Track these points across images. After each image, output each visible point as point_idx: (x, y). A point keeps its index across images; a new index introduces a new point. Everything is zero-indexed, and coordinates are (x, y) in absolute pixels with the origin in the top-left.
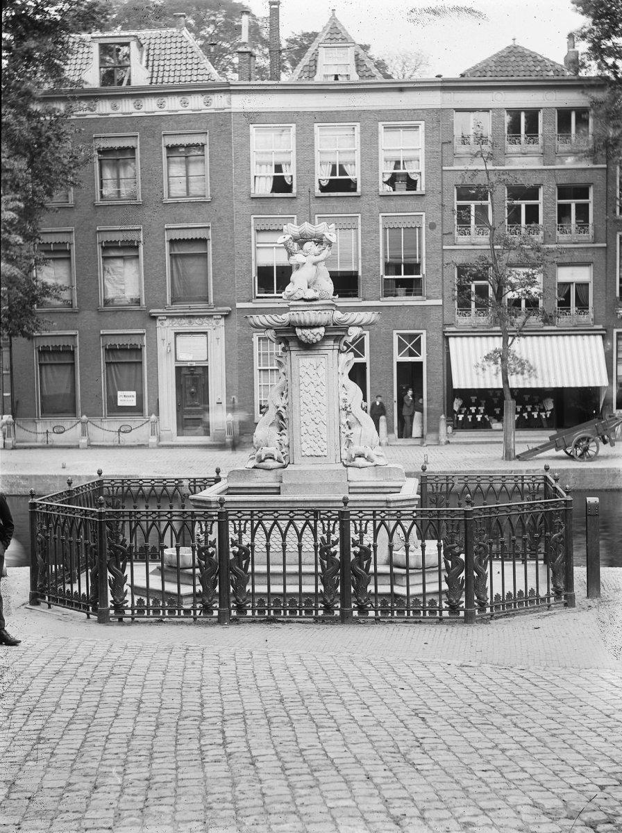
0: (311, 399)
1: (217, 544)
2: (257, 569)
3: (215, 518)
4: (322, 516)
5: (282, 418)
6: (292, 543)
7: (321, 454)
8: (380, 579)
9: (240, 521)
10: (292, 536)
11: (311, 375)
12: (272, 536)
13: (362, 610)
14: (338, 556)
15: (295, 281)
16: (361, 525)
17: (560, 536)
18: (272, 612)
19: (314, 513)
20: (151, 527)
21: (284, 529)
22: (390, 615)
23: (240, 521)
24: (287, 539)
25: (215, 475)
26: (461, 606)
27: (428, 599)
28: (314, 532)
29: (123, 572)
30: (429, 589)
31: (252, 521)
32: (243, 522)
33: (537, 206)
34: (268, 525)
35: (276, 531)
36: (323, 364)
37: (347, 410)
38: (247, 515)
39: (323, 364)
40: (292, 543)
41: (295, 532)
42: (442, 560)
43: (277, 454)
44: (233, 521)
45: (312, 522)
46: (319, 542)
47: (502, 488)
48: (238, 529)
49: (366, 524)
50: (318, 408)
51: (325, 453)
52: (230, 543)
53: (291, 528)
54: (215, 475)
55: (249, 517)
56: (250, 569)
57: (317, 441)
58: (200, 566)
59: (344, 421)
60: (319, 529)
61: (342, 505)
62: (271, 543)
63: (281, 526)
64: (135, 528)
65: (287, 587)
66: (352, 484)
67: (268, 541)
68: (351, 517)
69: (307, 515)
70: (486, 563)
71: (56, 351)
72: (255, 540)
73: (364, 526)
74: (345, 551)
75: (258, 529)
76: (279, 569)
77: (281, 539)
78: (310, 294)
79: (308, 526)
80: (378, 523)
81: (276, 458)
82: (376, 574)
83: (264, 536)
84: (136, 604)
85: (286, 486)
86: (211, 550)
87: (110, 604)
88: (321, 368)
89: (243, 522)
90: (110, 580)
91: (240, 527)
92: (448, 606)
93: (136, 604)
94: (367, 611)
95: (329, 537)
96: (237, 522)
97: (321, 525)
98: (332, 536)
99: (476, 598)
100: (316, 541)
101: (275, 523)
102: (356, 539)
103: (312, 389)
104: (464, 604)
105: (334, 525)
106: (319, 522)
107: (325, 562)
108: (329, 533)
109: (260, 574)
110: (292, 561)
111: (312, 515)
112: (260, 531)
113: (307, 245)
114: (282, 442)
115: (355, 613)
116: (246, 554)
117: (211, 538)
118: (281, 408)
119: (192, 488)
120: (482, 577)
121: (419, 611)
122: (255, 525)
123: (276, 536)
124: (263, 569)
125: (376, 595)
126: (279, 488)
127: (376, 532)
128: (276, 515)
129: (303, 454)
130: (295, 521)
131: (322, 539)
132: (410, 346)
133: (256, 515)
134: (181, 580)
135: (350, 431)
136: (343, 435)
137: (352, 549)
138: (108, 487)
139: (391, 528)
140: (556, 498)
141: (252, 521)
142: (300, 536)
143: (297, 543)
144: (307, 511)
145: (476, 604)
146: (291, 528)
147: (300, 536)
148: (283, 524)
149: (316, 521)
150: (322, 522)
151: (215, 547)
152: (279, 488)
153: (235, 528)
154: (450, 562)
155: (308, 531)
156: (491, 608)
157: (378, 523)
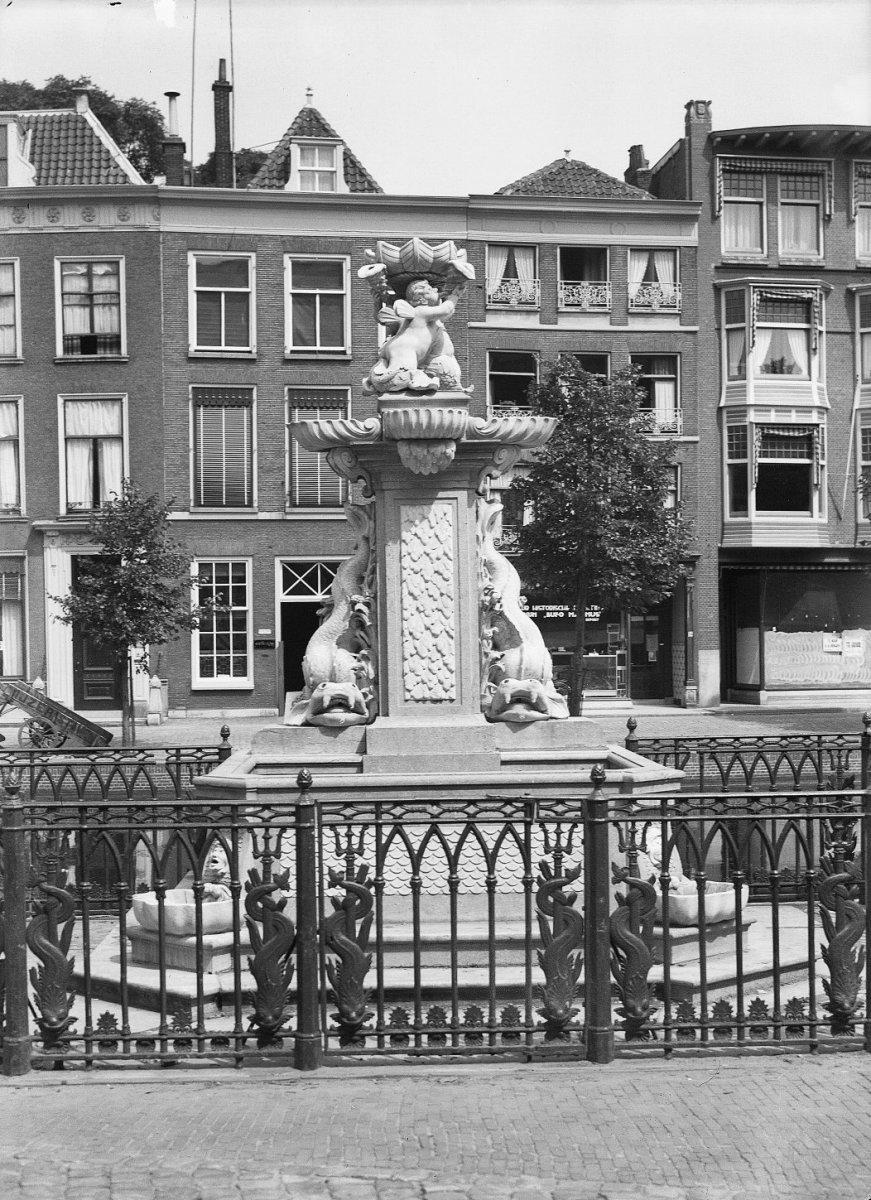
0: (423, 585)
2: (389, 934)
4: (543, 813)
5: (361, 625)
6: (433, 875)
7: (444, 695)
8: (389, 958)
9: (267, 829)
10: (472, 853)
12: (462, 859)
13: (350, 1033)
14: (578, 906)
18: (424, 1038)
21: (491, 845)
22: (195, 1050)
23: (267, 829)
24: (498, 866)
25: (219, 741)
26: (286, 1026)
27: (713, 996)
28: (525, 848)
29: (65, 951)
31: (379, 827)
32: (565, 827)
34: (416, 834)
36: (450, 517)
37: (490, 612)
40: (433, 875)
42: (534, 915)
43: (354, 694)
45: (520, 829)
46: (536, 872)
48: (344, 846)
49: (362, 834)
51: (453, 694)
52: (611, 875)
53: (434, 843)
54: (219, 741)
56: (373, 935)
57: (435, 669)
59: (488, 632)
60: (537, 846)
62: (460, 874)
63: (412, 839)
65: (386, 972)
67: (491, 869)
69: (508, 809)
72: (385, 869)
76: (443, 932)
77: (484, 867)
78: (421, 380)
79: (509, 836)
80: (387, 830)
81: (352, 702)
82: (382, 946)
84: (95, 1027)
85: (375, 760)
87: (615, 1017)
89: (356, 830)
91: (349, 842)
92: (544, 1020)
93: (95, 1027)
94: (363, 1037)
95: (558, 860)
96: (551, 827)
97: (541, 836)
98: (566, 857)
100: (528, 869)
101: (434, 830)
102: (337, 870)
105: (571, 832)
106: (535, 828)
108: (558, 853)
109: (397, 946)
110: (471, 916)
111: (518, 810)
112: (397, 849)
115: (334, 1044)
116: (363, 898)
119: (173, 768)
121: (517, 1034)
122: (384, 840)
123: (435, 859)
124: (406, 934)
127: (381, 852)
131: (253, 873)
132: (300, 579)
134: (168, 960)
135: (497, 654)
137: (613, 889)
138: (188, 763)
141: (379, 827)
142: (491, 859)
143: (447, 874)
146: (434, 843)
147: (491, 859)
148: (452, 833)
149: (528, 825)
150: (542, 825)
151: (287, 888)
153: (338, 844)
154: (832, 914)
155: (509, 845)
157: (387, 830)
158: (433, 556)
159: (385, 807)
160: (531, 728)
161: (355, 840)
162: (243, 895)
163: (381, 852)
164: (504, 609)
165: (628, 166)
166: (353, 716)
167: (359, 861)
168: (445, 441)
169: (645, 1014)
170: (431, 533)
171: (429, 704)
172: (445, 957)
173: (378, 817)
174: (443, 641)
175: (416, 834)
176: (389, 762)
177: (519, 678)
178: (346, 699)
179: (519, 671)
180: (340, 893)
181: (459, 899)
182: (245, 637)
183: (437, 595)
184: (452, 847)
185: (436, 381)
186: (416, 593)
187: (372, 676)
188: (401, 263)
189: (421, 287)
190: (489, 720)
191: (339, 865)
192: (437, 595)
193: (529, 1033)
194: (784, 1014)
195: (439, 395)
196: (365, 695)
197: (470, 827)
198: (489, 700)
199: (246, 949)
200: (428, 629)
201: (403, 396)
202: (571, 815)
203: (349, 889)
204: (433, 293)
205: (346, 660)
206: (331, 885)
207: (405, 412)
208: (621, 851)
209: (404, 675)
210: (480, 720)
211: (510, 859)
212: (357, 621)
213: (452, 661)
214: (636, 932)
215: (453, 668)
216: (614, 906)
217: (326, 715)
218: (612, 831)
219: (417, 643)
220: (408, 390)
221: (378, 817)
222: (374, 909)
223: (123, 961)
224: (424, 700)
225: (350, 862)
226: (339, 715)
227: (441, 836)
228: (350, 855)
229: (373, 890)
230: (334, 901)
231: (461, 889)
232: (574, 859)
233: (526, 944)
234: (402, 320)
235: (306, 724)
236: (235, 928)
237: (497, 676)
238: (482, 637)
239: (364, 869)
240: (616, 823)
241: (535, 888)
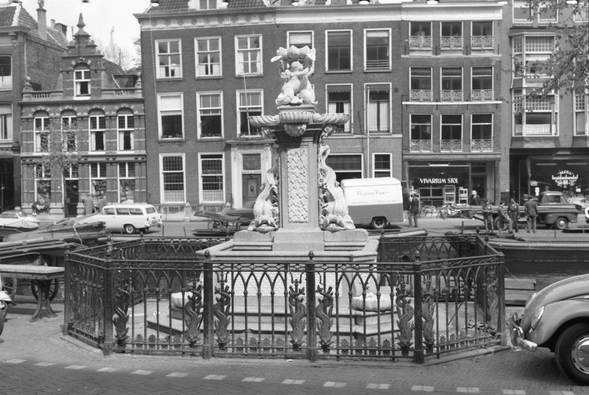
0: (296, 179)
1: (305, 292)
3: (202, 269)
4: (291, 268)
5: (274, 193)
9: (222, 272)
11: (296, 160)
14: (304, 303)
15: (285, 90)
16: (222, 276)
17: (494, 287)
19: (285, 266)
20: (341, 278)
24: (262, 287)
26: (411, 347)
28: (285, 281)
30: (383, 329)
31: (232, 272)
34: (350, 276)
35: (252, 281)
36: (306, 153)
38: (228, 267)
39: (306, 153)
43: (271, 220)
44: (216, 272)
46: (289, 290)
47: (432, 247)
49: (227, 275)
50: (302, 186)
51: (307, 220)
55: (230, 269)
56: (230, 310)
59: (322, 196)
61: (308, 259)
66: (326, 244)
68: (316, 269)
69: (279, 267)
70: (433, 309)
71: (498, 23)
73: (225, 276)
74: (311, 297)
78: (296, 100)
80: (340, 274)
81: (269, 223)
88: (304, 156)
90: (215, 322)
92: (400, 347)
95: (296, 286)
99: (424, 339)
101: (252, 274)
103: (297, 171)
104: (413, 346)
107: (401, 309)
108: (297, 283)
111: (282, 267)
112: (239, 280)
113: (295, 64)
114: (274, 212)
116: (227, 298)
117: (300, 287)
118: (274, 186)
120: (430, 320)
122: (339, 278)
124: (242, 310)
125: (338, 334)
126: (272, 246)
127: (233, 282)
128: (252, 267)
129: (290, 220)
130: (242, 273)
133: (236, 267)
135: (325, 205)
136: (320, 206)
139: (259, 279)
140: (486, 254)
141: (232, 272)
142: (273, 285)
144: (279, 264)
145: (424, 345)
147: (273, 285)
149: (286, 273)
152: (272, 246)
155: (279, 280)
156: (438, 348)
157: (340, 274)
158: (300, 167)
159: (235, 265)
160: (337, 233)
162: (395, 297)
163: (233, 282)
164: (328, 188)
166: (271, 228)
167: (226, 285)
168: (304, 123)
169: (328, 344)
170: (299, 158)
171: (298, 224)
172: (256, 319)
173: (232, 269)
174: (303, 200)
175: (246, 275)
176: (283, 246)
177: (333, 214)
178: (336, 220)
179: (334, 211)
180: (219, 296)
181: (248, 298)
183: (301, 182)
185: (301, 101)
186: (293, 181)
187: (278, 212)
188: (288, 56)
189: (297, 64)
190: (323, 230)
191: (219, 286)
192: (301, 182)
193: (393, 351)
194: (354, 345)
195: (302, 106)
196: (275, 220)
198: (322, 221)
199: (290, 315)
200: (297, 195)
201: (288, 106)
202: (302, 269)
203: (222, 295)
204: (300, 66)
205: (269, 206)
206: (216, 293)
207: (285, 114)
208: (218, 282)
209: (289, 213)
210: (318, 230)
211: (279, 283)
212: (273, 192)
213: (306, 207)
214: (194, 310)
215: (307, 210)
216: (215, 302)
217: (260, 227)
218: (214, 274)
219: (293, 201)
220: (290, 104)
221: (232, 269)
222: (231, 302)
223: (170, 317)
224: (296, 222)
225: (222, 285)
226: (264, 227)
227: (268, 276)
229: (230, 295)
230: (217, 299)
231: (248, 295)
232: (303, 285)
233: (285, 315)
234: (289, 77)
235: (254, 230)
237: (325, 213)
238: (319, 198)
239: (227, 287)
241: (288, 295)
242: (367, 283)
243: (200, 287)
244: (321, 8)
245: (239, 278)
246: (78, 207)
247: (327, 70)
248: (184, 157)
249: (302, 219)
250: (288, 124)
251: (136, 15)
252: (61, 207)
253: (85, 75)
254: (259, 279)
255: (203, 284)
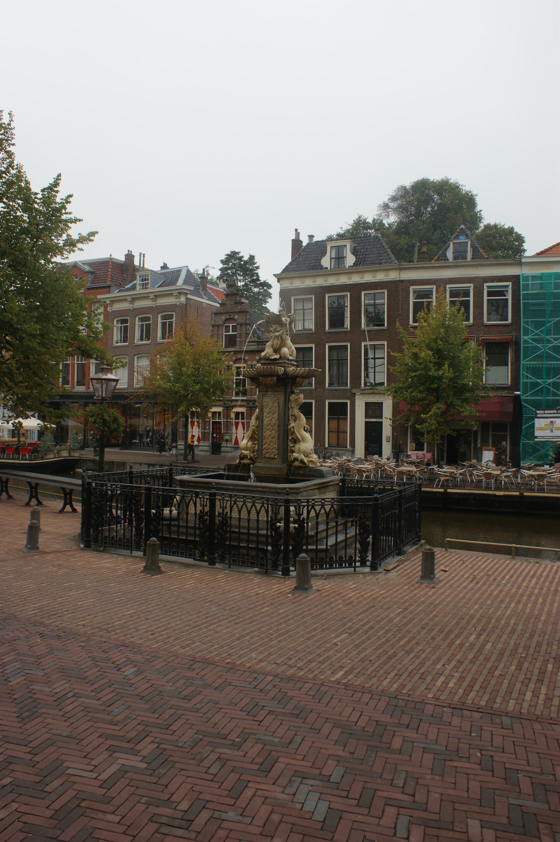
12: (242, 512)
16: (223, 503)
33: (450, 297)
34: (258, 506)
41: (255, 511)
44: (220, 500)
45: (265, 505)
51: (276, 457)
58: (200, 529)
64: (196, 501)
75: (191, 503)
77: (247, 515)
79: (263, 508)
83: (237, 512)
86: (206, 517)
89: (205, 500)
127: (231, 508)
131: (201, 510)
146: (253, 508)
148: (249, 505)
155: (263, 510)
157: (233, 503)
161: (225, 504)
163: (231, 508)
165: (289, 260)
173: (308, 503)
182: (380, 425)
184: (249, 509)
197: (263, 504)
213: (276, 446)
225: (223, 511)
227: (246, 506)
228: (224, 508)
236: (267, 530)
239: (227, 513)
240: (220, 500)
242: (189, 504)
243: (303, 518)
244: (444, 265)
245: (313, 510)
246: (222, 445)
247: (327, 328)
248: (314, 402)
249: (272, 456)
250: (262, 376)
251: (275, 275)
252: (208, 444)
253: (232, 329)
254: (240, 506)
255: (283, 516)
